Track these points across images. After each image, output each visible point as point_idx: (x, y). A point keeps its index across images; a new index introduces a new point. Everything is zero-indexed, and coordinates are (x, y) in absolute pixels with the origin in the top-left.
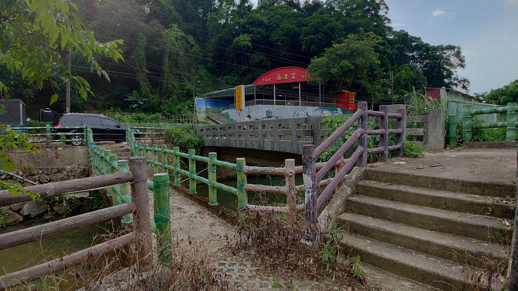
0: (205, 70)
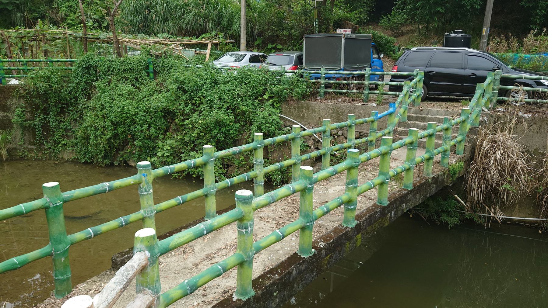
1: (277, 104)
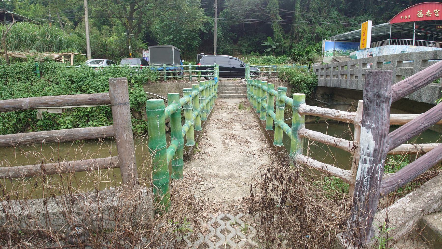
0: (337, 12)
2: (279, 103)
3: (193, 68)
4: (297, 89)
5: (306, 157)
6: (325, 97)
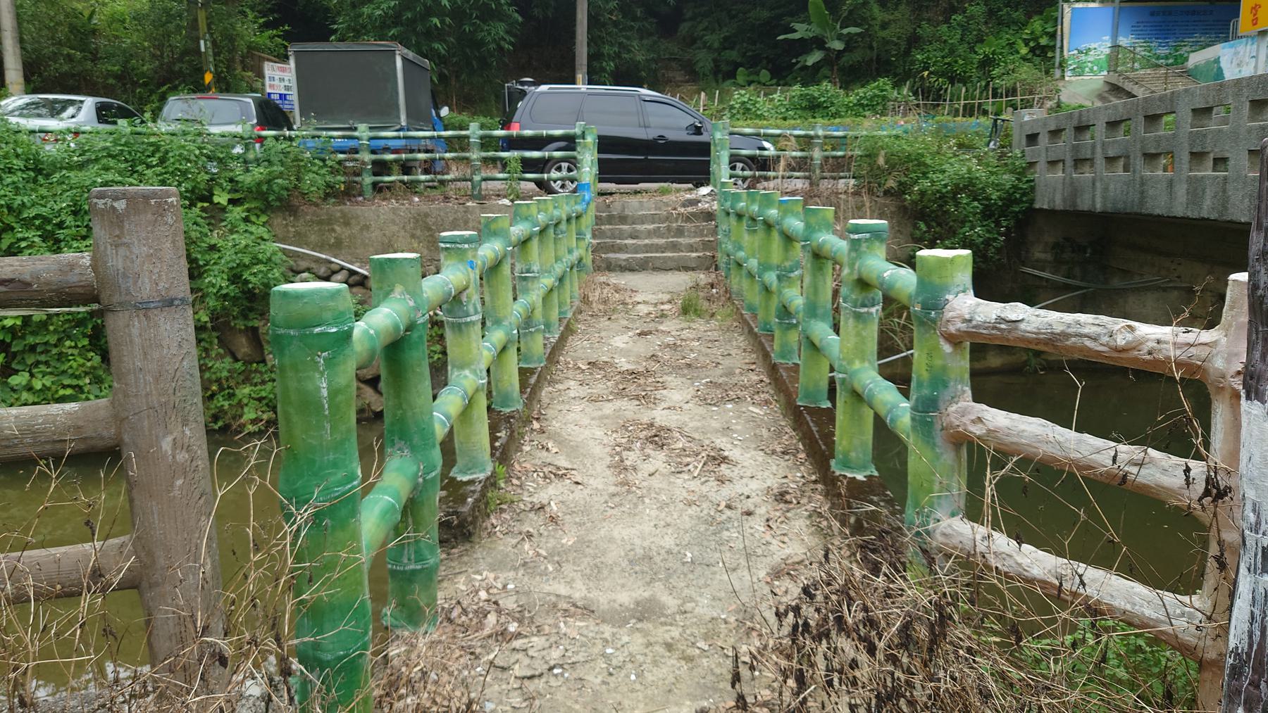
1: (258, 216)
2: (852, 291)
3: (486, 143)
4: (939, 224)
5: (982, 530)
6: (1067, 255)
